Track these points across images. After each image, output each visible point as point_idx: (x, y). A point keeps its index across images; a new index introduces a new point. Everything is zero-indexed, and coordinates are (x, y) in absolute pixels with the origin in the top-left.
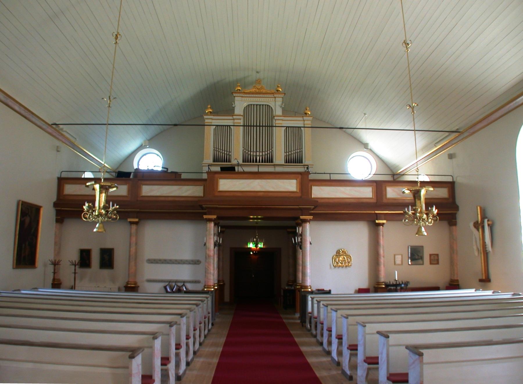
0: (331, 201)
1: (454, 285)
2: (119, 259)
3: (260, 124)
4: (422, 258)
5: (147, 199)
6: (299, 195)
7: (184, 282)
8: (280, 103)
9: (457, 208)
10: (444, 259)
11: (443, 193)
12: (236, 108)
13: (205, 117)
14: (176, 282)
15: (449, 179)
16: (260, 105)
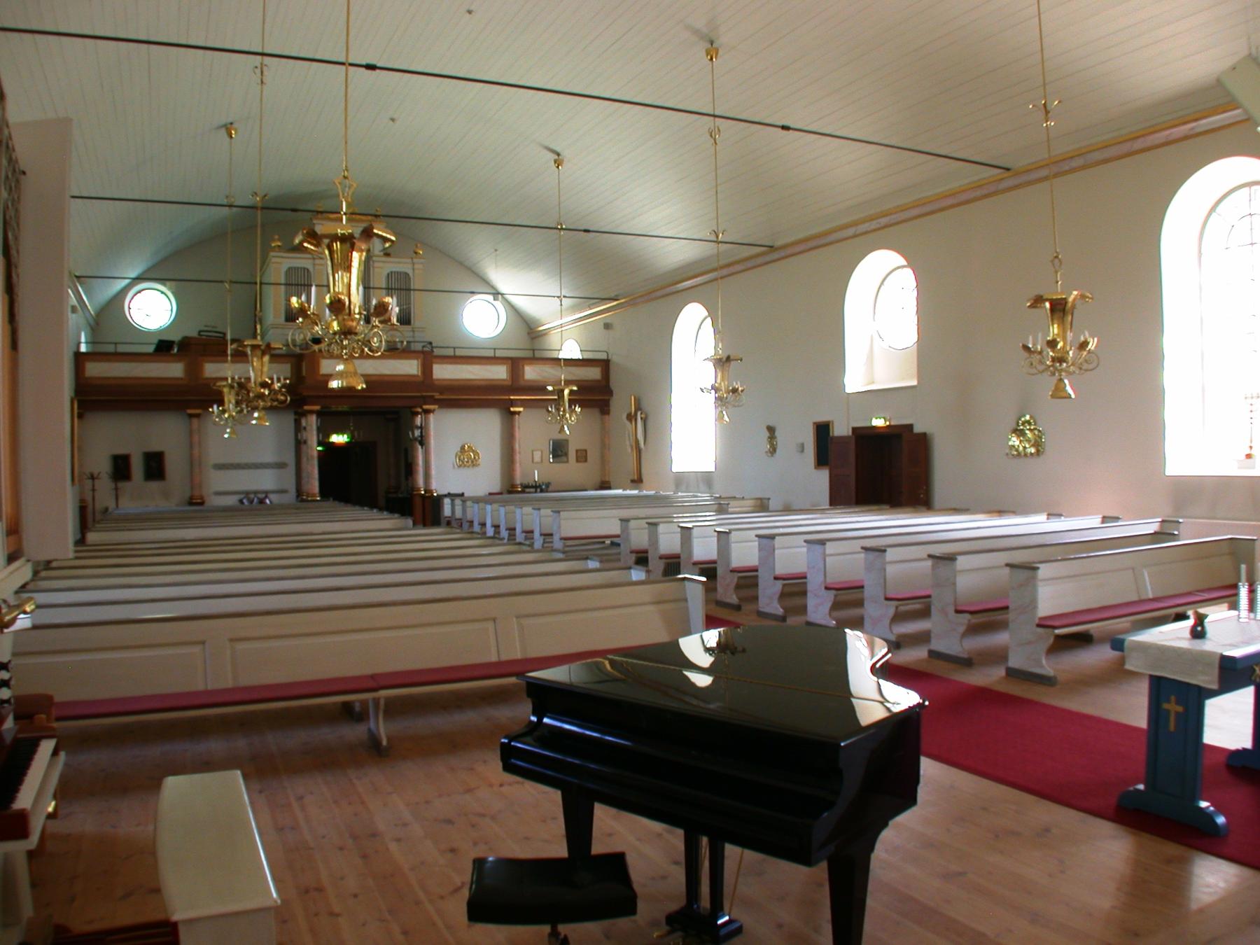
1: (605, 486)
2: (174, 465)
4: (566, 454)
6: (421, 379)
7: (267, 493)
9: (610, 393)
10: (593, 456)
11: (594, 373)
13: (272, 254)
14: (256, 493)
15: (603, 356)
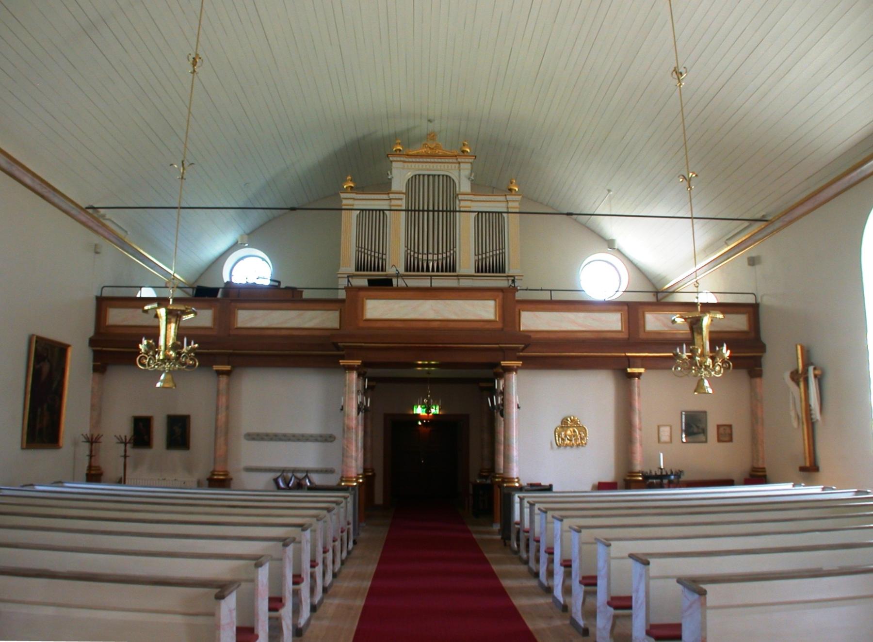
0: (553, 336)
1: (757, 477)
2: (199, 432)
3: (433, 207)
4: (704, 431)
5: (245, 332)
6: (500, 326)
7: (307, 471)
8: (467, 172)
9: (762, 348)
10: (740, 433)
11: (739, 323)
12: (393, 181)
13: (343, 195)
14: (294, 471)
15: (750, 299)
16: (434, 176)
